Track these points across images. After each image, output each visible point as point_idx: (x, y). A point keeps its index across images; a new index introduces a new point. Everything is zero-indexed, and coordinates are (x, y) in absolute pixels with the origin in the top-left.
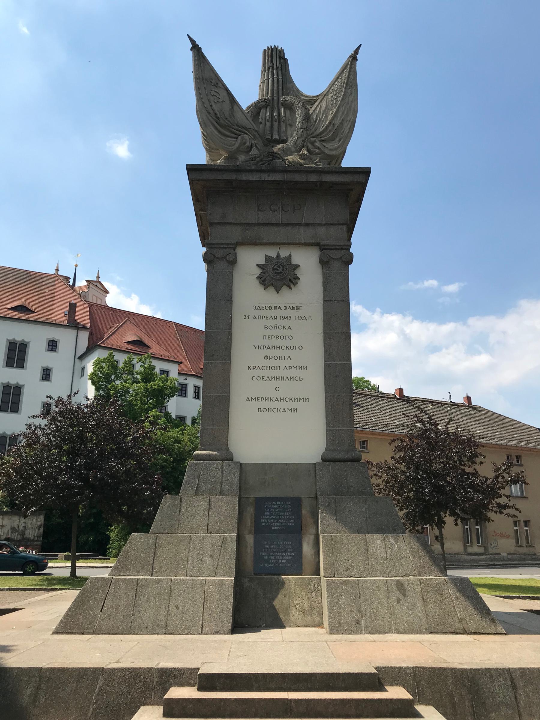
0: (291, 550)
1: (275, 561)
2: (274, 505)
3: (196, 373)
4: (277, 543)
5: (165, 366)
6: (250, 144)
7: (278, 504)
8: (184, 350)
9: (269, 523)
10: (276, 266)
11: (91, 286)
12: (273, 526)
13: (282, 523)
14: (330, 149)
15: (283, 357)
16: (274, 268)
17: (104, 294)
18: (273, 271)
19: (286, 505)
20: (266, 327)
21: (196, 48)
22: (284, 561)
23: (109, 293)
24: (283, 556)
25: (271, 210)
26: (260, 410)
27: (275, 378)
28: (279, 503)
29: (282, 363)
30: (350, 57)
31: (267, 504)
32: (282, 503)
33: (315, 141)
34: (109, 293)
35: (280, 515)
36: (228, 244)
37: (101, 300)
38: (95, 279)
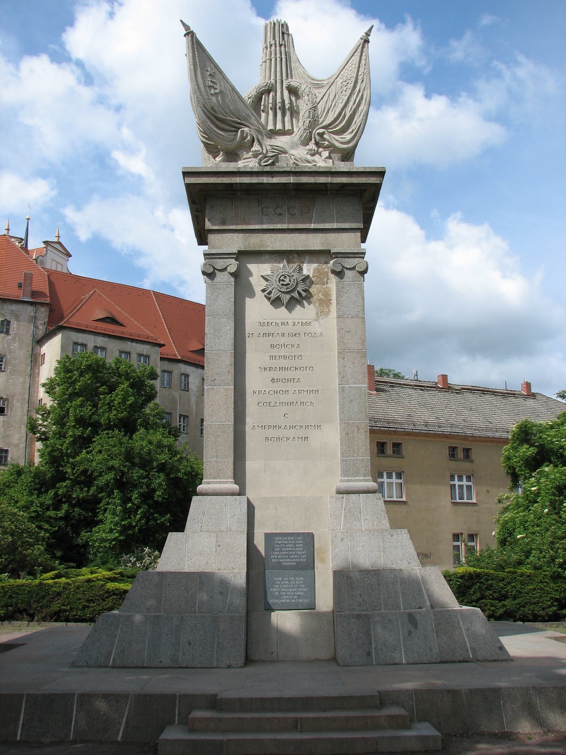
0: (303, 586)
1: (286, 597)
2: (284, 540)
3: (183, 357)
4: (288, 579)
5: (144, 349)
6: (252, 138)
7: (289, 540)
8: (169, 336)
9: (279, 559)
10: (283, 277)
11: (49, 248)
12: (284, 562)
13: (293, 558)
14: (342, 143)
15: (292, 380)
16: (281, 279)
17: (66, 258)
18: (279, 282)
19: (297, 540)
20: (272, 346)
21: (190, 34)
22: (296, 597)
23: (71, 256)
24: (294, 592)
25: (277, 214)
26: (267, 439)
27: (284, 403)
28: (290, 538)
29: (290, 387)
30: (361, 39)
31: (277, 540)
32: (292, 538)
33: (324, 133)
34: (71, 256)
35: (291, 551)
36: (229, 254)
37: (62, 265)
38: (56, 240)
